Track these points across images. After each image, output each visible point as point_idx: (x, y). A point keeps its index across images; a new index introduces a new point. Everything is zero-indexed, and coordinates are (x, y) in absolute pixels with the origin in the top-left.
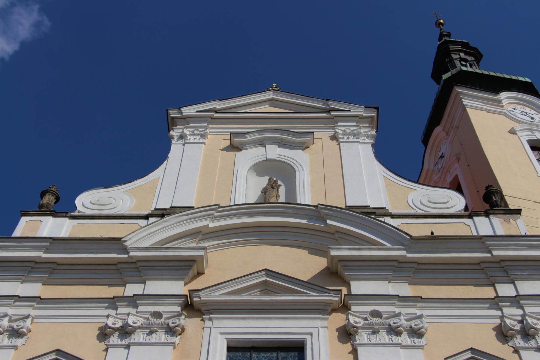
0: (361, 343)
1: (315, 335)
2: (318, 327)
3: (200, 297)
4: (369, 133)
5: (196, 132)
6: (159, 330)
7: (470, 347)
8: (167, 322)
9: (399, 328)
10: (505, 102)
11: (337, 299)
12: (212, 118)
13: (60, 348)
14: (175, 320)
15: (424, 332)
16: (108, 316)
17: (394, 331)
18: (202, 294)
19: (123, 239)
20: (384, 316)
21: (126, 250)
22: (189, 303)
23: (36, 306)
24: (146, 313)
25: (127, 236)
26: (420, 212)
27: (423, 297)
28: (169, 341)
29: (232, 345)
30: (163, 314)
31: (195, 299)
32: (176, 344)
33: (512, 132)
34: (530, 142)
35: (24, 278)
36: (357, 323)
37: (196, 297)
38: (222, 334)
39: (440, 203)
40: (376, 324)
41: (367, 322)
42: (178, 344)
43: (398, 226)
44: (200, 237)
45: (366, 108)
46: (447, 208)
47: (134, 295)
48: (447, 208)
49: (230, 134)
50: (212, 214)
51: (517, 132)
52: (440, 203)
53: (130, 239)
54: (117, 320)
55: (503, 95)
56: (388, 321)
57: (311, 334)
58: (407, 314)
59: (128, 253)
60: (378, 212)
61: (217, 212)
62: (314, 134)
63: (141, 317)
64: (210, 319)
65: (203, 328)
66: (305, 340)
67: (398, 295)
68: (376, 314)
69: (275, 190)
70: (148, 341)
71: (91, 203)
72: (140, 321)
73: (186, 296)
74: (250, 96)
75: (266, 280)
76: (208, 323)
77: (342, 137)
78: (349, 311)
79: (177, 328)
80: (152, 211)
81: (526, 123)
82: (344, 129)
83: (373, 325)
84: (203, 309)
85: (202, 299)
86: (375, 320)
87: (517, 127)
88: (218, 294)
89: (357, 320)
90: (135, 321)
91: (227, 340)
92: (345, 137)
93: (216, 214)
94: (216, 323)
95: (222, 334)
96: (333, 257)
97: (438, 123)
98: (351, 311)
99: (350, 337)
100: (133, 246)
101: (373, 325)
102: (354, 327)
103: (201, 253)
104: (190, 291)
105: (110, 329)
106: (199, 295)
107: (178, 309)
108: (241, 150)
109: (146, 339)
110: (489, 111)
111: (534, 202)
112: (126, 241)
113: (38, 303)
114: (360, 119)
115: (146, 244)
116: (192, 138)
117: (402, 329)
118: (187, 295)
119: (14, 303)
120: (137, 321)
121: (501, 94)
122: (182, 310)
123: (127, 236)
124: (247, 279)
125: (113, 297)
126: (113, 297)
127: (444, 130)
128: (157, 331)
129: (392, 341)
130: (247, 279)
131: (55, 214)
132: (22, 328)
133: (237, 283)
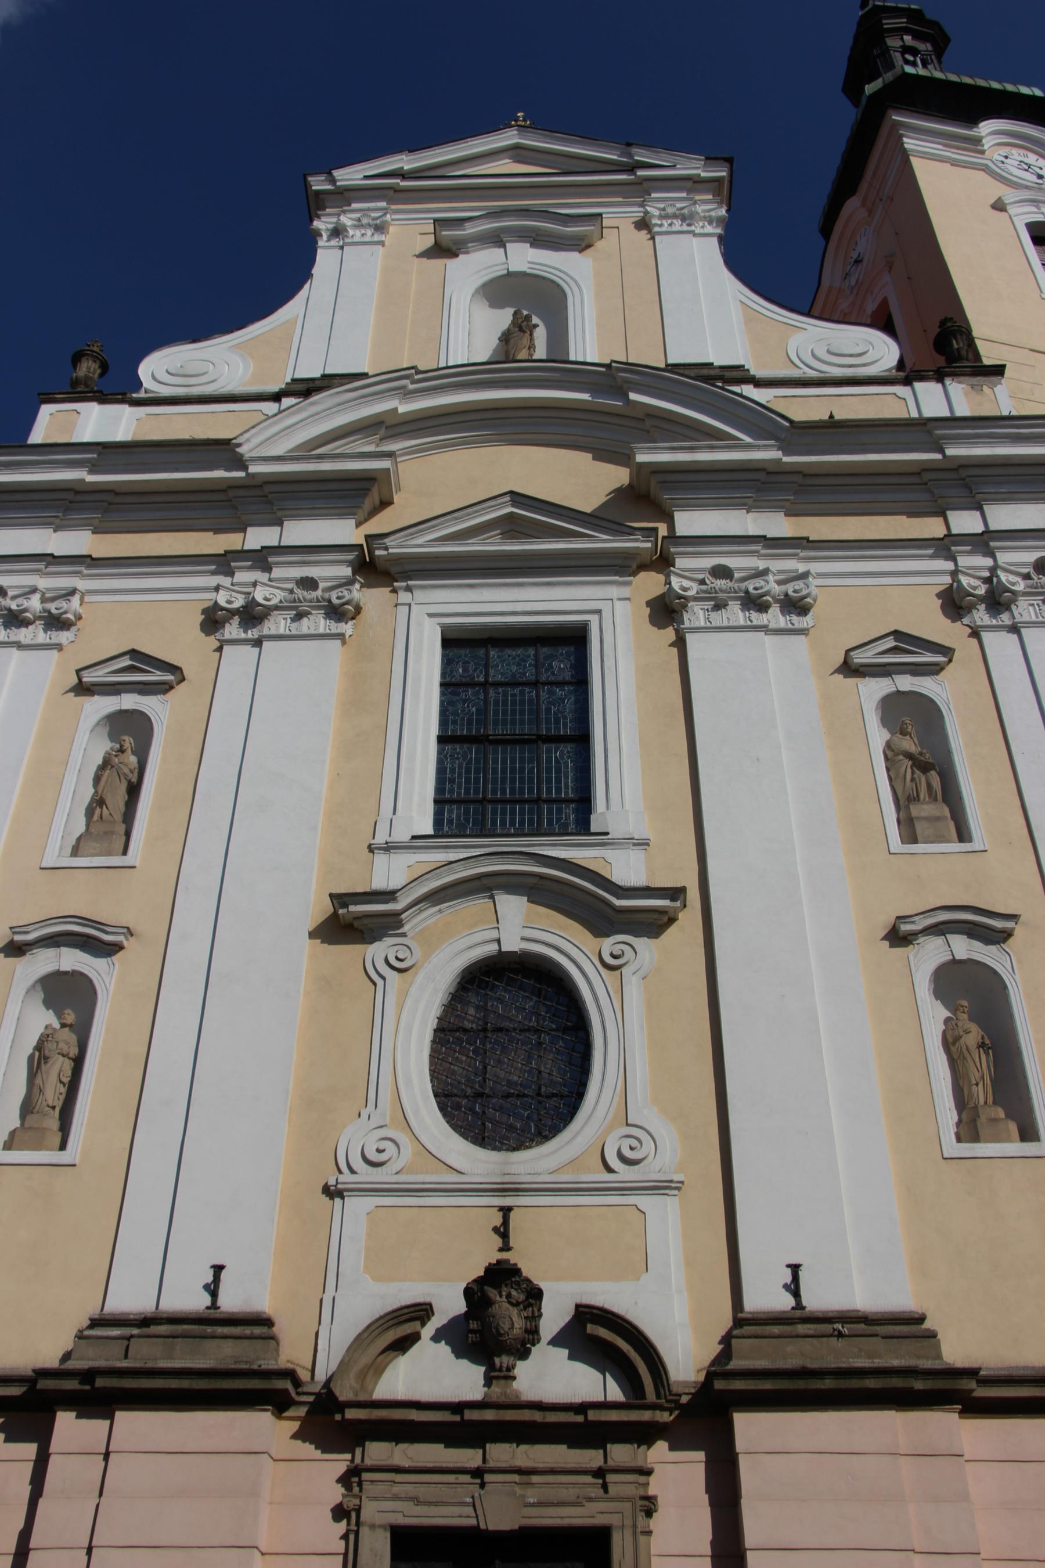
0: (692, 626)
1: (606, 615)
2: (612, 600)
3: (386, 549)
4: (713, 214)
5: (365, 221)
6: (313, 612)
7: (892, 630)
8: (327, 595)
9: (765, 598)
10: (987, 143)
11: (649, 545)
12: (397, 190)
13: (135, 648)
14: (342, 592)
15: (810, 603)
16: (217, 589)
17: (754, 603)
18: (391, 541)
19: (234, 441)
20: (736, 575)
21: (240, 463)
22: (368, 560)
23: (85, 572)
24: (287, 580)
25: (241, 434)
26: (811, 374)
27: (810, 539)
28: (334, 631)
29: (449, 636)
30: (319, 581)
31: (378, 553)
32: (347, 636)
33: (999, 206)
34: (1031, 227)
35: (58, 521)
36: (685, 589)
37: (378, 548)
38: (430, 615)
39: (851, 356)
40: (721, 591)
41: (704, 587)
42: (350, 636)
43: (767, 402)
44: (382, 432)
45: (708, 161)
46: (864, 365)
47: (263, 548)
48: (864, 365)
49: (434, 223)
50: (404, 387)
51: (1008, 207)
52: (851, 356)
53: (248, 440)
54: (234, 594)
55: (987, 128)
56: (743, 585)
57: (599, 612)
58: (780, 572)
59: (245, 468)
60: (728, 374)
61: (413, 382)
62: (602, 218)
63: (278, 588)
64: (409, 589)
65: (396, 606)
66: (587, 624)
67: (764, 537)
68: (722, 572)
69: (527, 335)
70: (294, 632)
71: (169, 373)
72: (277, 596)
73: (359, 548)
74: (471, 141)
75: (512, 513)
76: (404, 597)
77: (659, 222)
78: (672, 568)
79: (346, 606)
80: (287, 384)
81: (1027, 187)
82: (662, 206)
83: (716, 592)
84: (394, 570)
85: (391, 551)
86: (721, 583)
87: (1009, 195)
88: (420, 541)
89: (686, 583)
90: (269, 597)
91: (440, 627)
92: (664, 222)
93: (411, 387)
94: (419, 595)
95: (430, 615)
96: (642, 465)
97: (852, 191)
98: (674, 567)
99: (673, 615)
100: (254, 454)
101: (716, 592)
102: (680, 597)
103: (385, 464)
104: (368, 537)
105: (224, 612)
106: (385, 544)
107: (347, 571)
108: (457, 256)
109: (291, 628)
110: (955, 163)
111: (1031, 350)
112: (239, 445)
113: (89, 567)
114: (696, 184)
115: (280, 449)
116: (358, 233)
117: (771, 599)
118: (362, 545)
119: (46, 568)
120: (272, 596)
121: (982, 125)
122: (354, 573)
123: (241, 434)
124: (476, 512)
125: (223, 552)
126: (223, 552)
127: (863, 204)
128: (310, 613)
129: (751, 621)
130: (476, 512)
131: (103, 397)
132: (66, 612)
133: (456, 519)
